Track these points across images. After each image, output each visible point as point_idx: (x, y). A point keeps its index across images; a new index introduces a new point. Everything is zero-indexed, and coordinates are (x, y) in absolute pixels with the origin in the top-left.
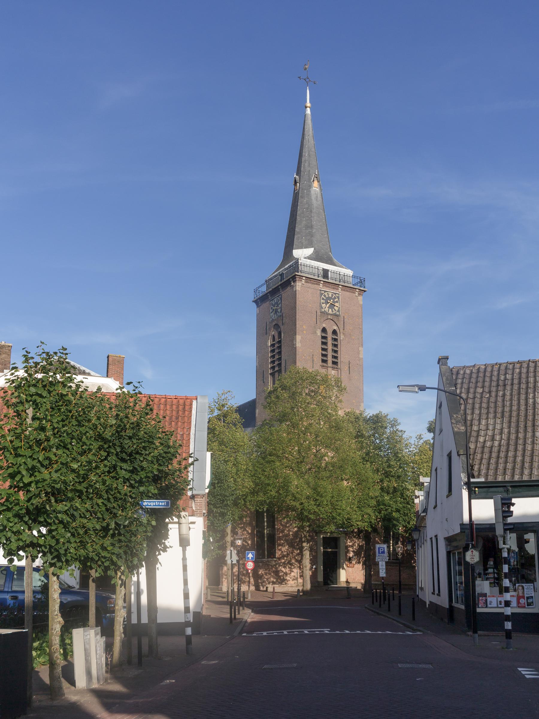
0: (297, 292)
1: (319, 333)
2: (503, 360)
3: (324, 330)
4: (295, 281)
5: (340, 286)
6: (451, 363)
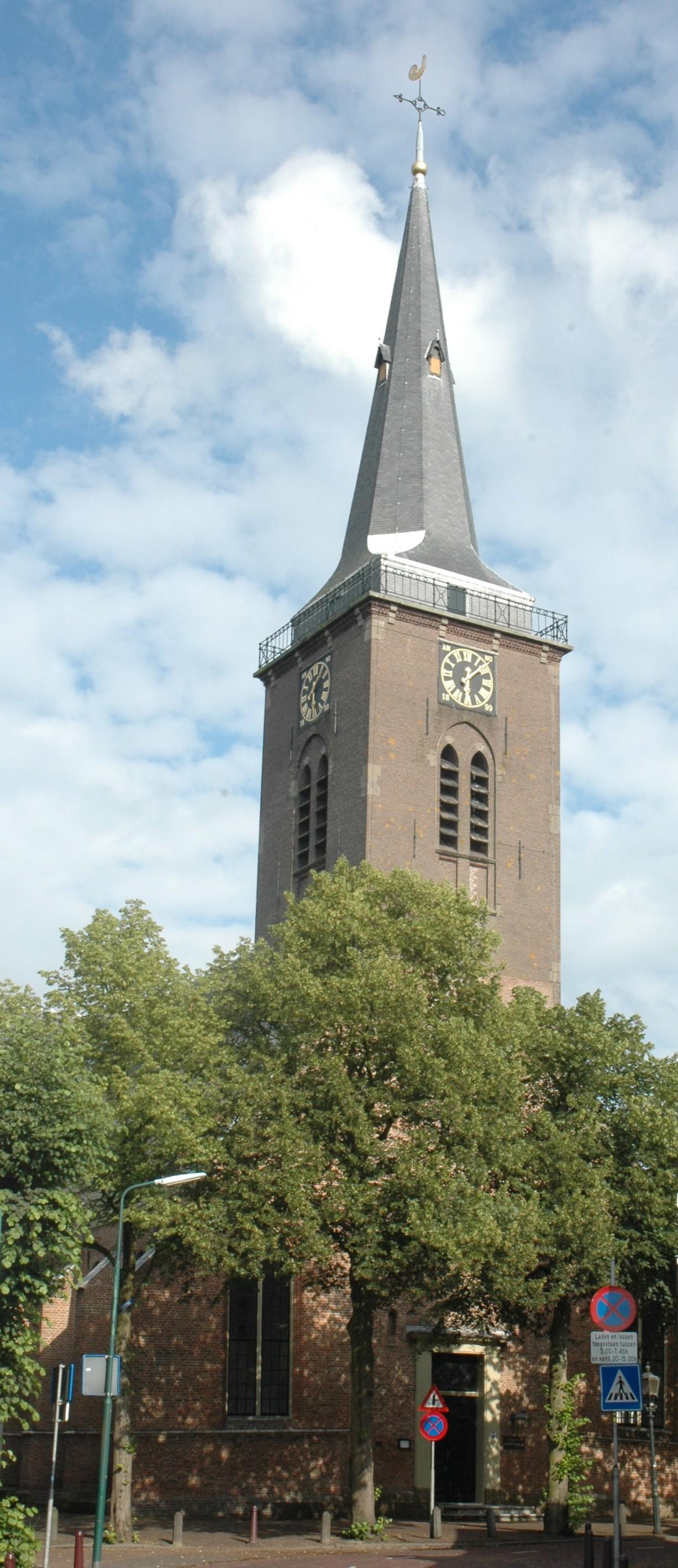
0: (374, 646)
1: (434, 759)
3: (448, 753)
4: (367, 615)
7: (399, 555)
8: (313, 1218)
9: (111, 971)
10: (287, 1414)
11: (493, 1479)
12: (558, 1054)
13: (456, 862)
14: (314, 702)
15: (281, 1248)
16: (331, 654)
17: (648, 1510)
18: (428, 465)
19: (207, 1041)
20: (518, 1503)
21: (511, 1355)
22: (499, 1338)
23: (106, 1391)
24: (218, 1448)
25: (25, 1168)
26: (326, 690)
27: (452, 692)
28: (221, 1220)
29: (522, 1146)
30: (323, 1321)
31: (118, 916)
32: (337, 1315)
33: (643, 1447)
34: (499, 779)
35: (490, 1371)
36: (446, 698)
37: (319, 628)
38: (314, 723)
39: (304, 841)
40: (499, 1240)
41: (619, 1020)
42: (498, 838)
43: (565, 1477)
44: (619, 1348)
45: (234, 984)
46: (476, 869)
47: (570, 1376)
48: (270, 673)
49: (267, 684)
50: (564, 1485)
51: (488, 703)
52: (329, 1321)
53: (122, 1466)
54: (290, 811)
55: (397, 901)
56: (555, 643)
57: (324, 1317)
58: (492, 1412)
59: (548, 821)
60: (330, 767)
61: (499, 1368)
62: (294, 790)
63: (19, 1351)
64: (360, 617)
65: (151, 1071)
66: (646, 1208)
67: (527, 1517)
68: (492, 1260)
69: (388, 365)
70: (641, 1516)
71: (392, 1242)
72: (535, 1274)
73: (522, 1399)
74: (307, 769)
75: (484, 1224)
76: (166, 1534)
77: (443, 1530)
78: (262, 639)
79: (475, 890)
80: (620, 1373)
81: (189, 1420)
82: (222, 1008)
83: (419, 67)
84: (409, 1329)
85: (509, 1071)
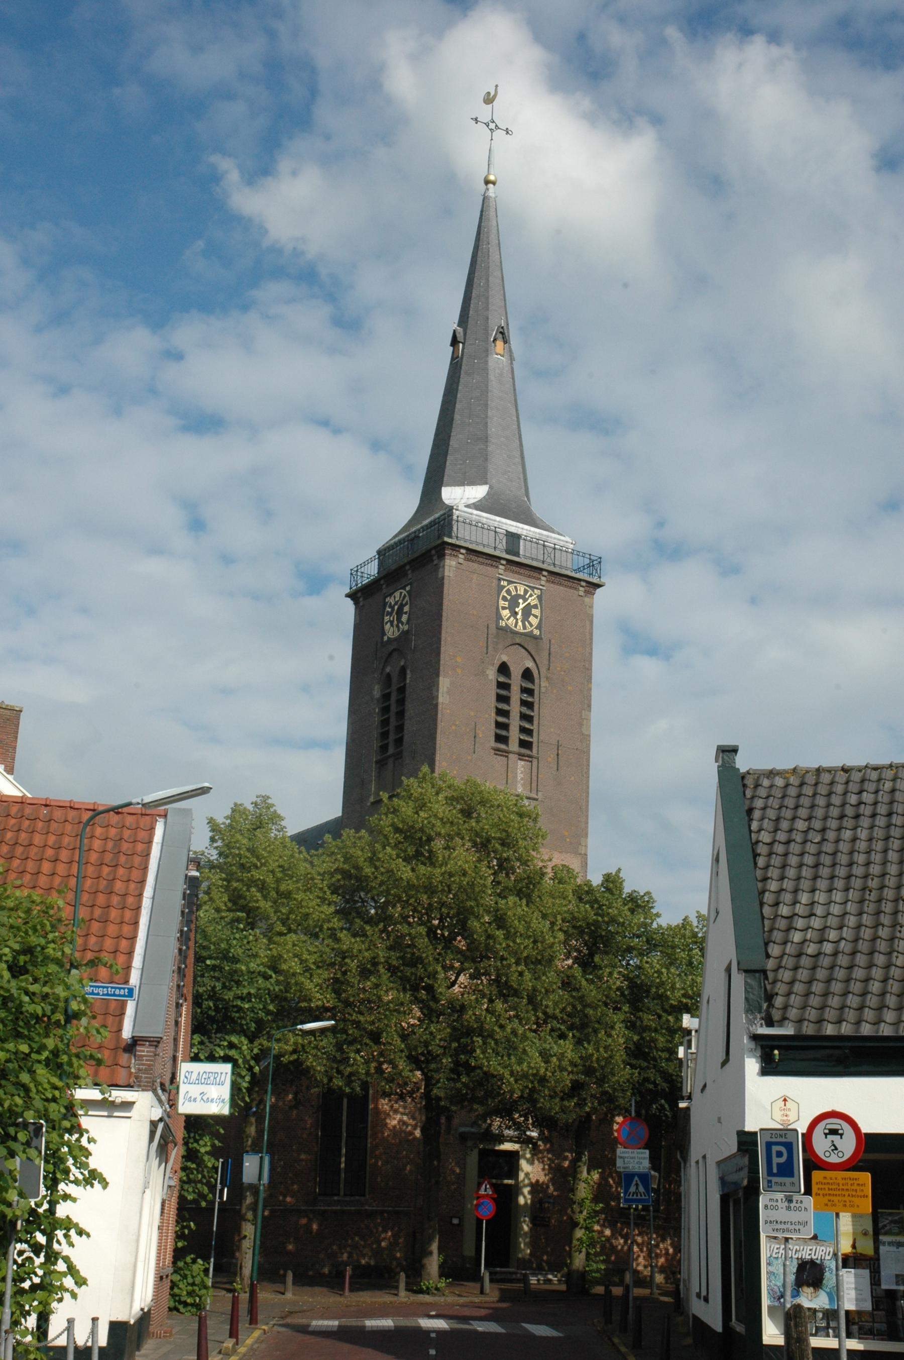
0: (446, 581)
1: (492, 674)
2: (810, 762)
3: (504, 669)
4: (442, 556)
5: (545, 573)
6: (742, 763)
7: (468, 506)
8: (402, 1051)
9: (248, 854)
10: (364, 1195)
11: (524, 1250)
12: (588, 924)
13: (507, 757)
14: (395, 622)
15: (376, 1072)
16: (411, 584)
17: (646, 1277)
18: (492, 430)
19: (322, 910)
20: (543, 1269)
21: (541, 1152)
22: (532, 1138)
23: (260, 1180)
24: (310, 1221)
25: (212, 1020)
26: (406, 613)
27: (508, 619)
28: (331, 1049)
29: (559, 995)
30: (394, 1122)
31: (250, 808)
32: (405, 1118)
33: (643, 1227)
34: (543, 690)
35: (523, 1164)
36: (502, 624)
37: (402, 563)
38: (395, 640)
39: (385, 735)
40: (542, 1071)
41: (634, 895)
42: (541, 738)
43: (584, 1250)
44: (636, 1160)
45: (341, 865)
46: (523, 763)
47: (588, 1173)
48: (359, 595)
49: (356, 603)
50: (583, 1256)
51: (536, 628)
52: (399, 1122)
53: (247, 1234)
54: (374, 709)
55: (468, 805)
56: (591, 580)
57: (395, 1119)
58: (525, 1197)
59: (581, 725)
60: (409, 676)
61: (531, 1162)
62: (377, 693)
63: (203, 1150)
64: (435, 557)
65: (281, 934)
66: (653, 1045)
67: (550, 1280)
68: (537, 1085)
69: (461, 345)
70: (641, 1281)
71: (461, 1069)
72: (568, 1095)
73: (548, 1187)
74: (389, 675)
75: (531, 1058)
76: (280, 1287)
77: (490, 1288)
78: (353, 566)
79: (522, 779)
80: (636, 1178)
81: (288, 1199)
82: (333, 884)
83: (492, 94)
84: (462, 1129)
85: (552, 940)
